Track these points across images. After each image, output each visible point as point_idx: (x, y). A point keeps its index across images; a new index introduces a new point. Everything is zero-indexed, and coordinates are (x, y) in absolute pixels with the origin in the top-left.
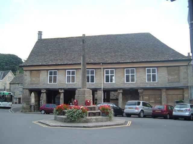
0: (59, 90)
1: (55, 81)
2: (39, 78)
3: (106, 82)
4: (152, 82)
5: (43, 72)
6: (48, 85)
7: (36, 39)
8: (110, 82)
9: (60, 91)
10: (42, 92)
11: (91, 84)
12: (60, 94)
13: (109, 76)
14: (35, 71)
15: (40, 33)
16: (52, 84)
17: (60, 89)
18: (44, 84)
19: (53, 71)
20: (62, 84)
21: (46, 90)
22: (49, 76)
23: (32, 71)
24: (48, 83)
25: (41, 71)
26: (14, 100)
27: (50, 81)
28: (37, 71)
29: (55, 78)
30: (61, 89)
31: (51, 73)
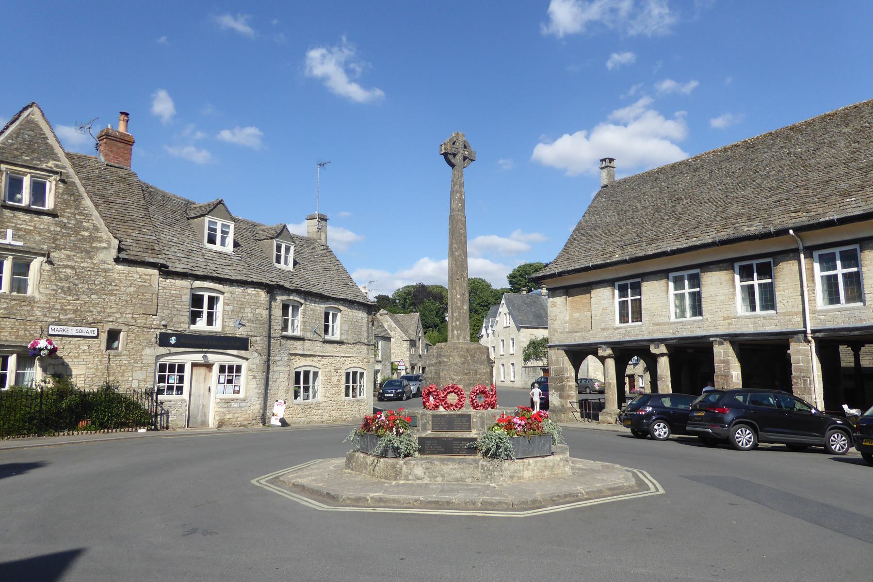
1: (638, 316)
6: (617, 331)
9: (653, 350)
11: (621, 328)
16: (628, 327)
18: (603, 329)
21: (612, 349)
22: (158, 374)
27: (623, 318)
29: (637, 304)
31: (623, 292)
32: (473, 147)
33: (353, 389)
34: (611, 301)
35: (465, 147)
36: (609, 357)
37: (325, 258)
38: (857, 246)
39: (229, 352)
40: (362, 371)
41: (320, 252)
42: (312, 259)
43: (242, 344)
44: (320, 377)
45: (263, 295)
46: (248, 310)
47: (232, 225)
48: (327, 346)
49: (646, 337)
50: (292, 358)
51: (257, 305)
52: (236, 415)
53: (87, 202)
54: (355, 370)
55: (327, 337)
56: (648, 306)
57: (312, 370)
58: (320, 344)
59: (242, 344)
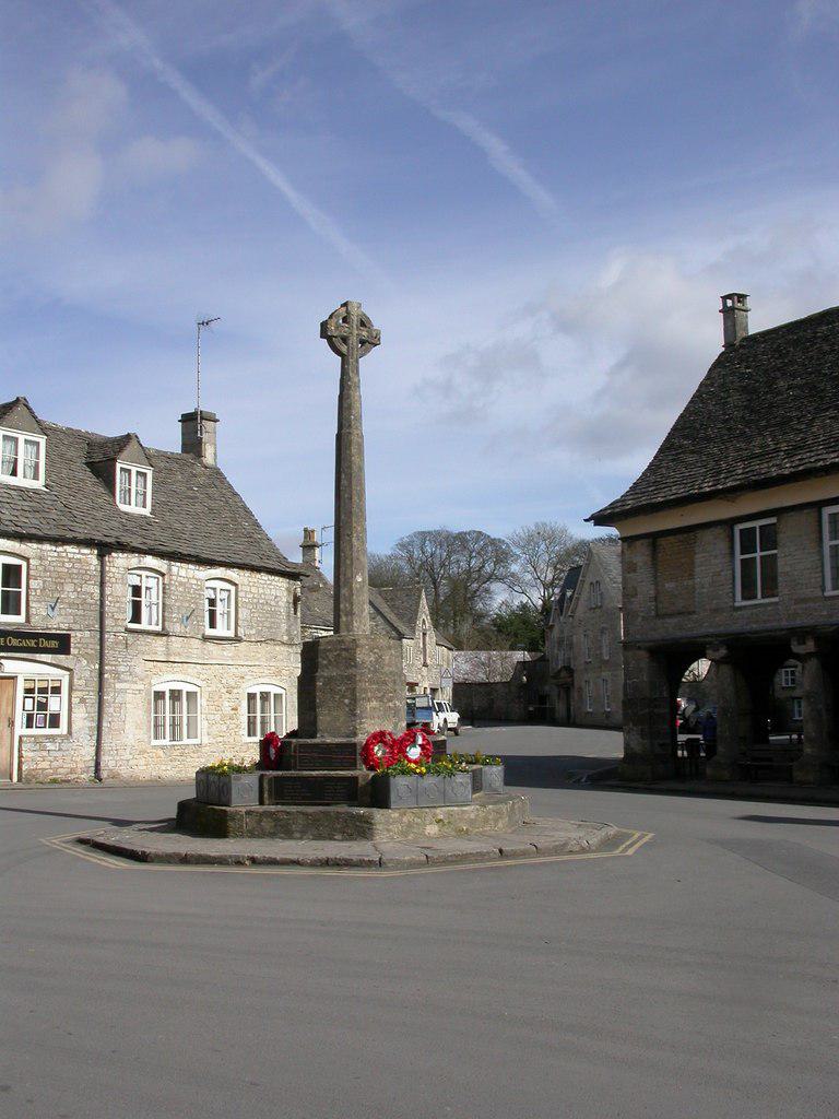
0: (462, 721)
1: (770, 587)
2: (691, 576)
3: (744, 598)
4: (762, 601)
5: (707, 536)
7: (712, 342)
8: (166, 742)
9: (797, 648)
10: (797, 657)
12: (628, 703)
13: (761, 557)
14: (671, 538)
15: (732, 309)
17: (793, 631)
18: (716, 610)
19: (757, 524)
20: (804, 600)
23: (662, 542)
24: (739, 602)
25: (700, 534)
26: (793, 711)
27: (748, 592)
28: (680, 537)
29: (770, 564)
30: (802, 633)
32: (377, 324)
33: (173, 725)
34: (728, 559)
35: (363, 324)
36: (810, 655)
37: (210, 491)
38: (773, 520)
39: (38, 657)
40: (279, 691)
41: (201, 480)
42: (190, 493)
43: (62, 644)
44: (202, 702)
45: (90, 556)
46: (69, 588)
47: (42, 440)
48: (210, 646)
49: (784, 624)
50: (572, 721)
51: (83, 576)
52: (55, 764)
53: (495, 146)
54: (265, 689)
55: (210, 632)
56: (788, 569)
57: (186, 688)
58: (196, 643)
59: (62, 644)
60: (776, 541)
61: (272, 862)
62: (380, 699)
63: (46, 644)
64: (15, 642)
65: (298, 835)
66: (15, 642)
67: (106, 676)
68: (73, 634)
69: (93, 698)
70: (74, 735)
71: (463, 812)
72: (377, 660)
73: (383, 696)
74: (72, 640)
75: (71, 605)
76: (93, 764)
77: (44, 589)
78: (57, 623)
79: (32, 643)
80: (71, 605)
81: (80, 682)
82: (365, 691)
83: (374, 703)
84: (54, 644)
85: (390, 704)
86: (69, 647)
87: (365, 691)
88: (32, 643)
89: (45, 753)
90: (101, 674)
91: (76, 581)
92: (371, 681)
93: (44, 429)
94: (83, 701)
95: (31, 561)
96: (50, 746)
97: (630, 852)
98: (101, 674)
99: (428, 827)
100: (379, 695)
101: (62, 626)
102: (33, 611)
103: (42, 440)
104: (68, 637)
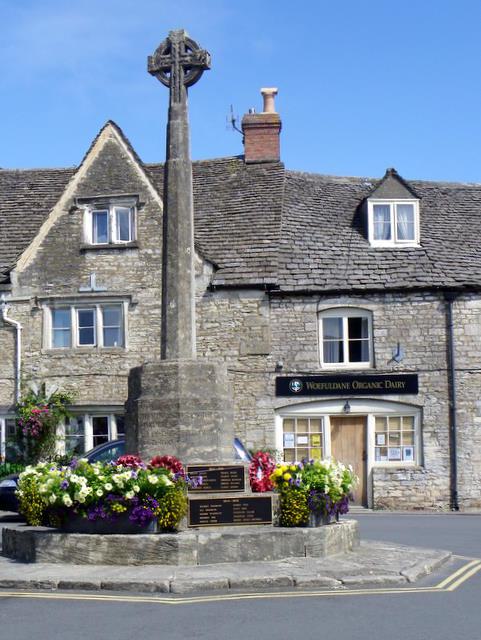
39: (385, 397)
45: (434, 305)
46: (415, 333)
52: (407, 492)
59: (409, 384)
60: (177, 203)
61: (86, 587)
62: (163, 424)
63: (392, 385)
64: (360, 385)
65: (132, 560)
66: (360, 385)
67: (459, 411)
68: (420, 375)
69: (445, 432)
70: (427, 467)
71: (129, 541)
72: (162, 386)
73: (166, 421)
74: (420, 380)
75: (417, 348)
76: (448, 493)
77: (389, 335)
78: (406, 364)
79: (378, 385)
80: (417, 348)
81: (431, 418)
82: (146, 416)
83: (157, 428)
84: (400, 385)
85: (174, 429)
86: (417, 386)
87: (146, 416)
88: (378, 385)
89: (397, 483)
90: (452, 410)
91: (421, 326)
92: (153, 406)
93: (411, 189)
94: (434, 434)
95: (374, 313)
96: (401, 476)
97: (451, 589)
98: (452, 410)
99: (92, 554)
100: (162, 420)
101: (408, 368)
102: (378, 356)
103: (416, 204)
104: (415, 378)
